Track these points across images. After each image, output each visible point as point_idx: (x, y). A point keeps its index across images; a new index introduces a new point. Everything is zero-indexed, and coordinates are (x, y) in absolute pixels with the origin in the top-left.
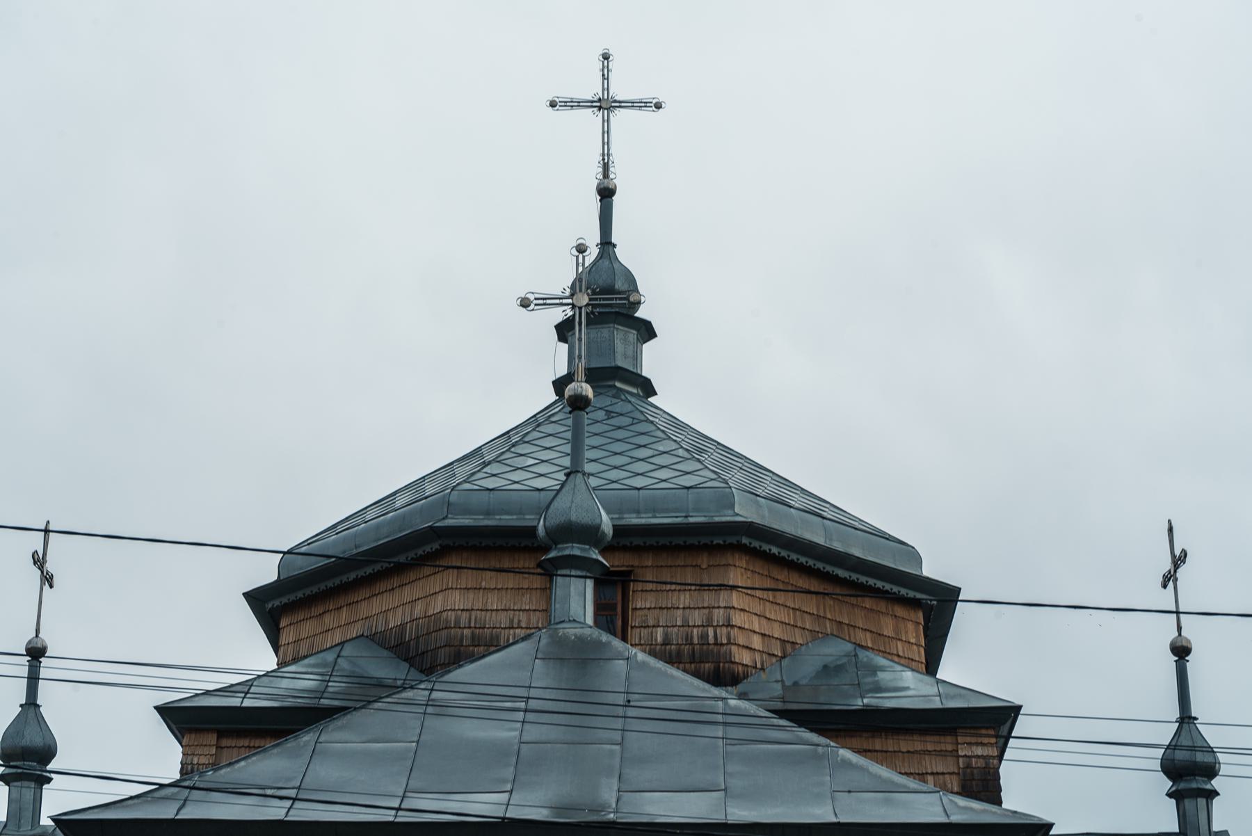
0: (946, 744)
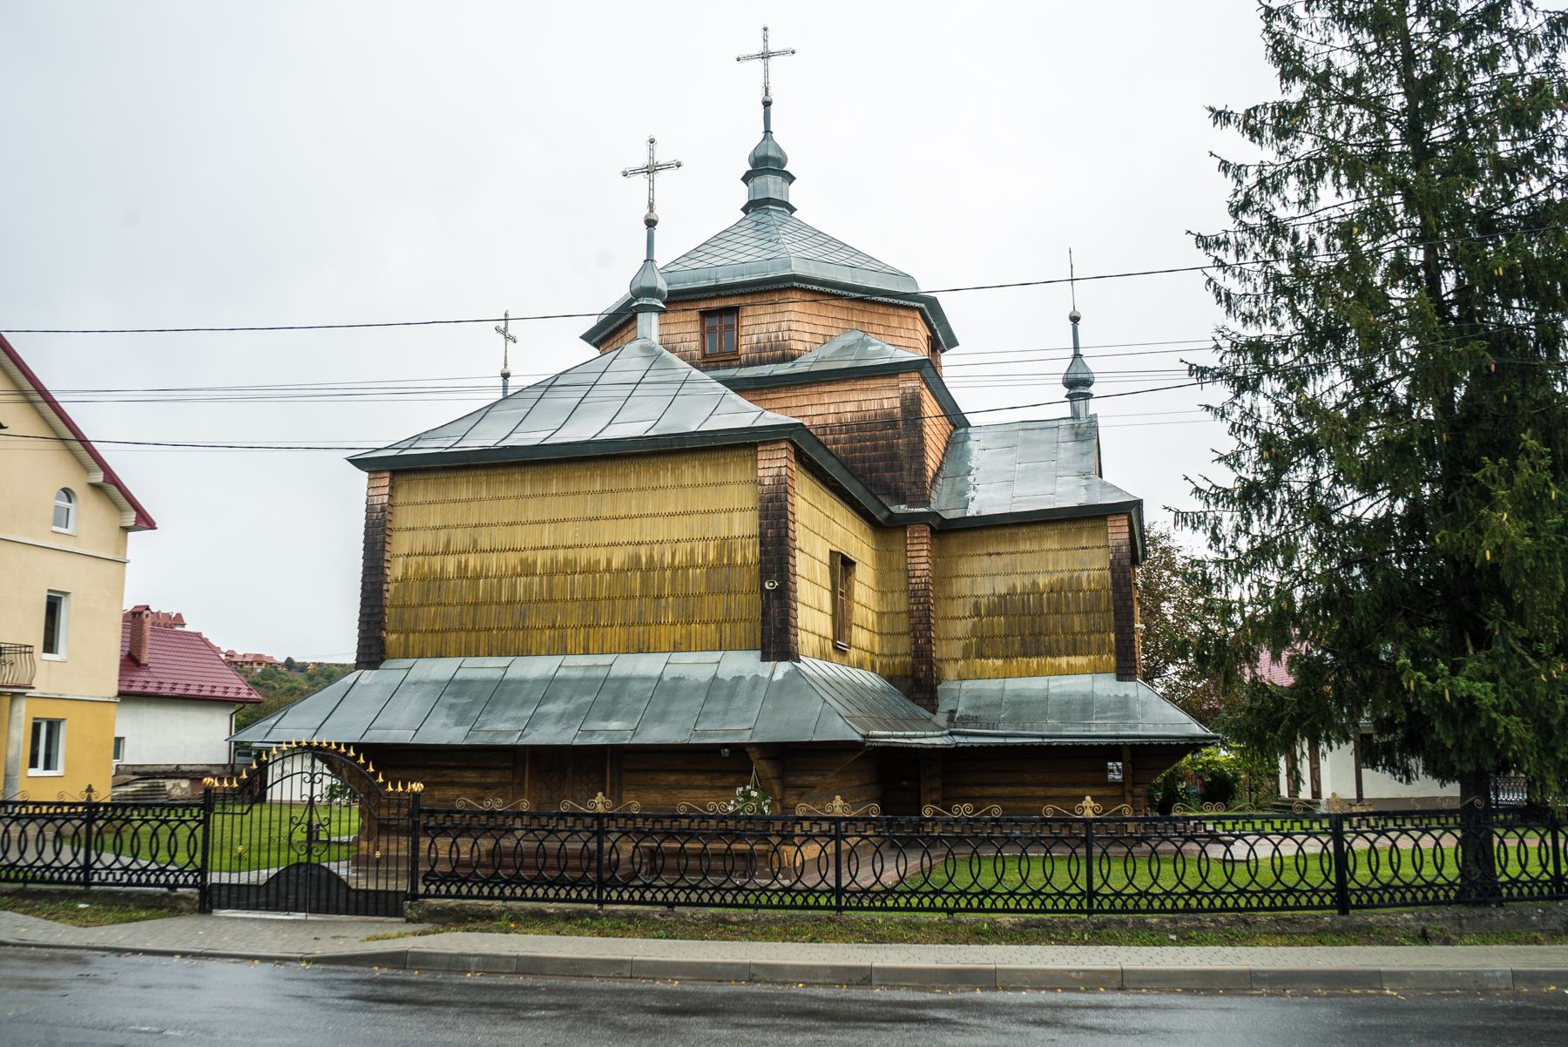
0: (894, 381)
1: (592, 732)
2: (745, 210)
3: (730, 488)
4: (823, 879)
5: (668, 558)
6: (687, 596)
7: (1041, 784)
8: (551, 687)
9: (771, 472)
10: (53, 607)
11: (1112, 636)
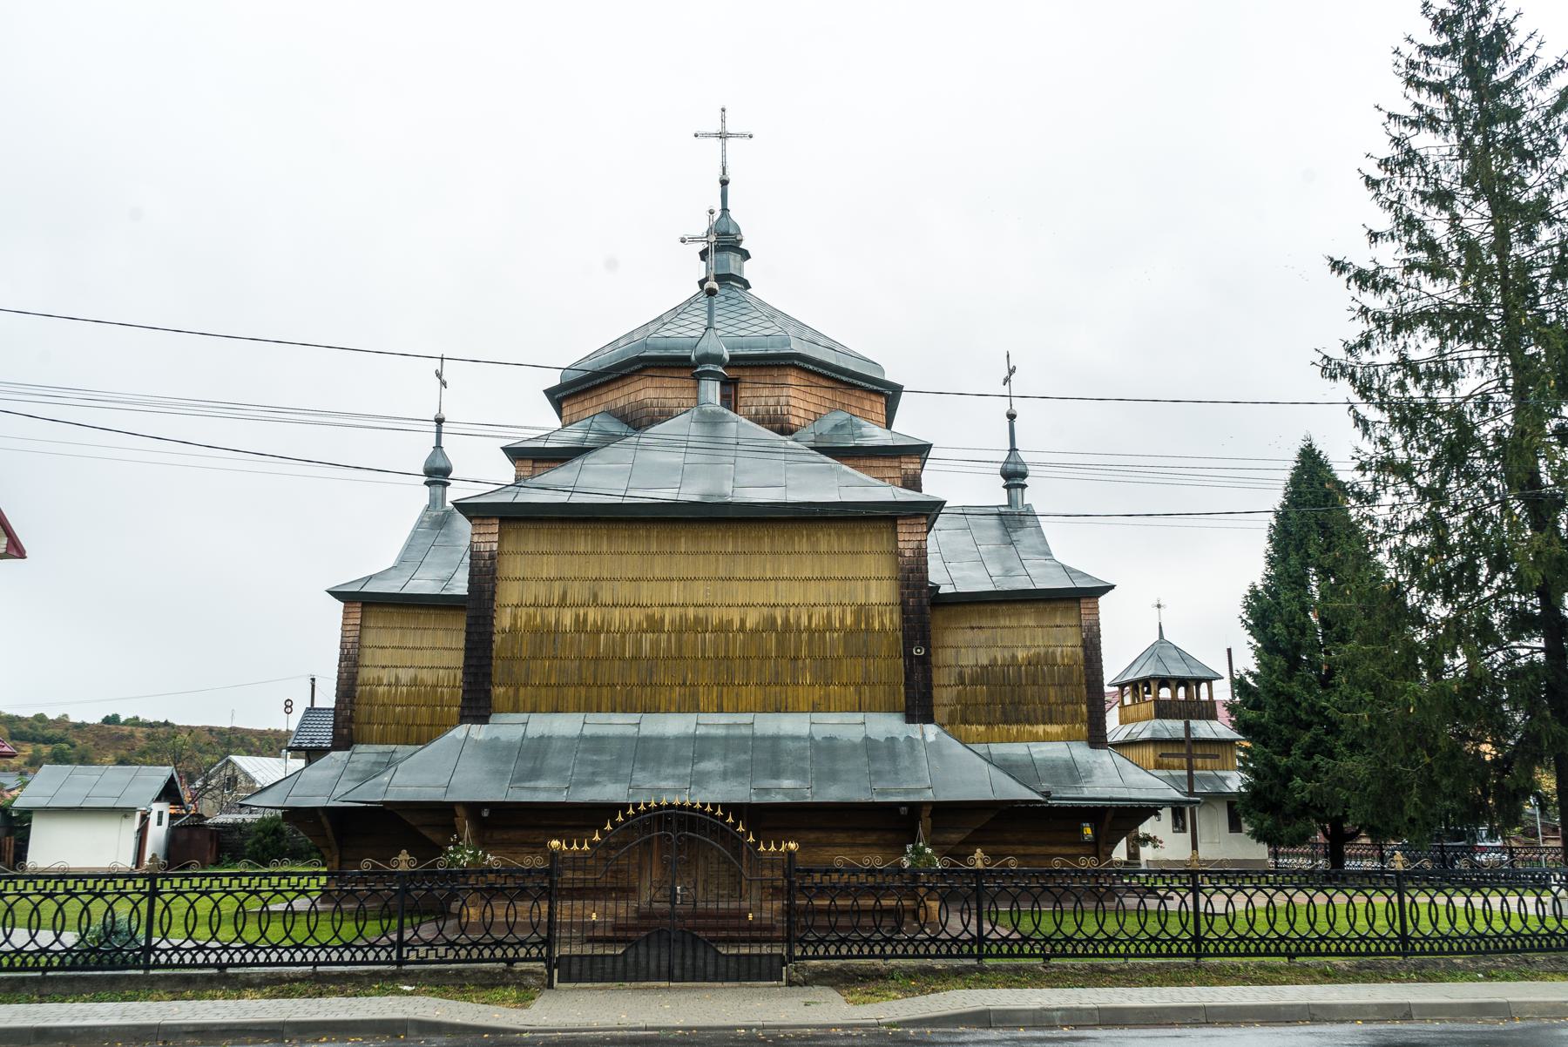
1: (767, 791)
3: (866, 557)
4: (966, 928)
5: (804, 620)
6: (825, 658)
7: (1022, 843)
8: (700, 746)
9: (911, 545)
10: (1229, 651)
11: (1084, 708)
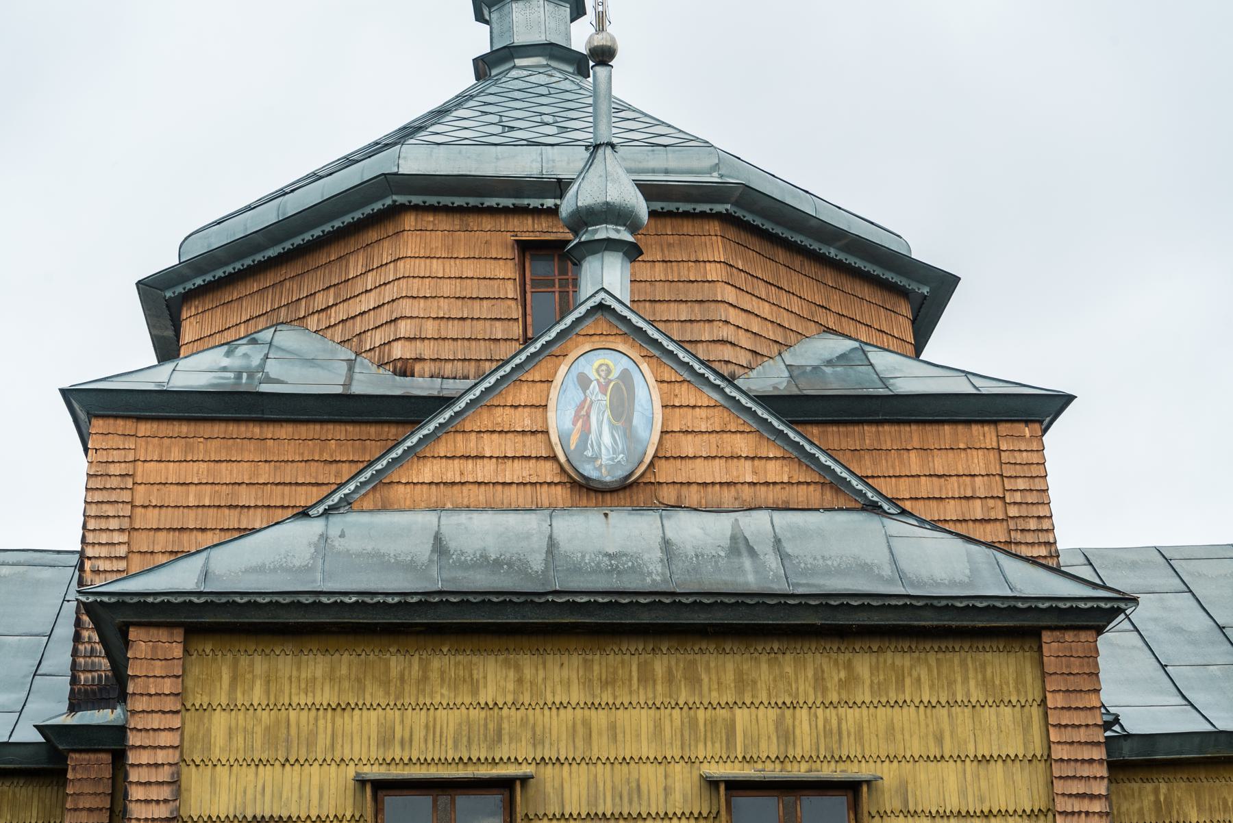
2: (484, 66)
